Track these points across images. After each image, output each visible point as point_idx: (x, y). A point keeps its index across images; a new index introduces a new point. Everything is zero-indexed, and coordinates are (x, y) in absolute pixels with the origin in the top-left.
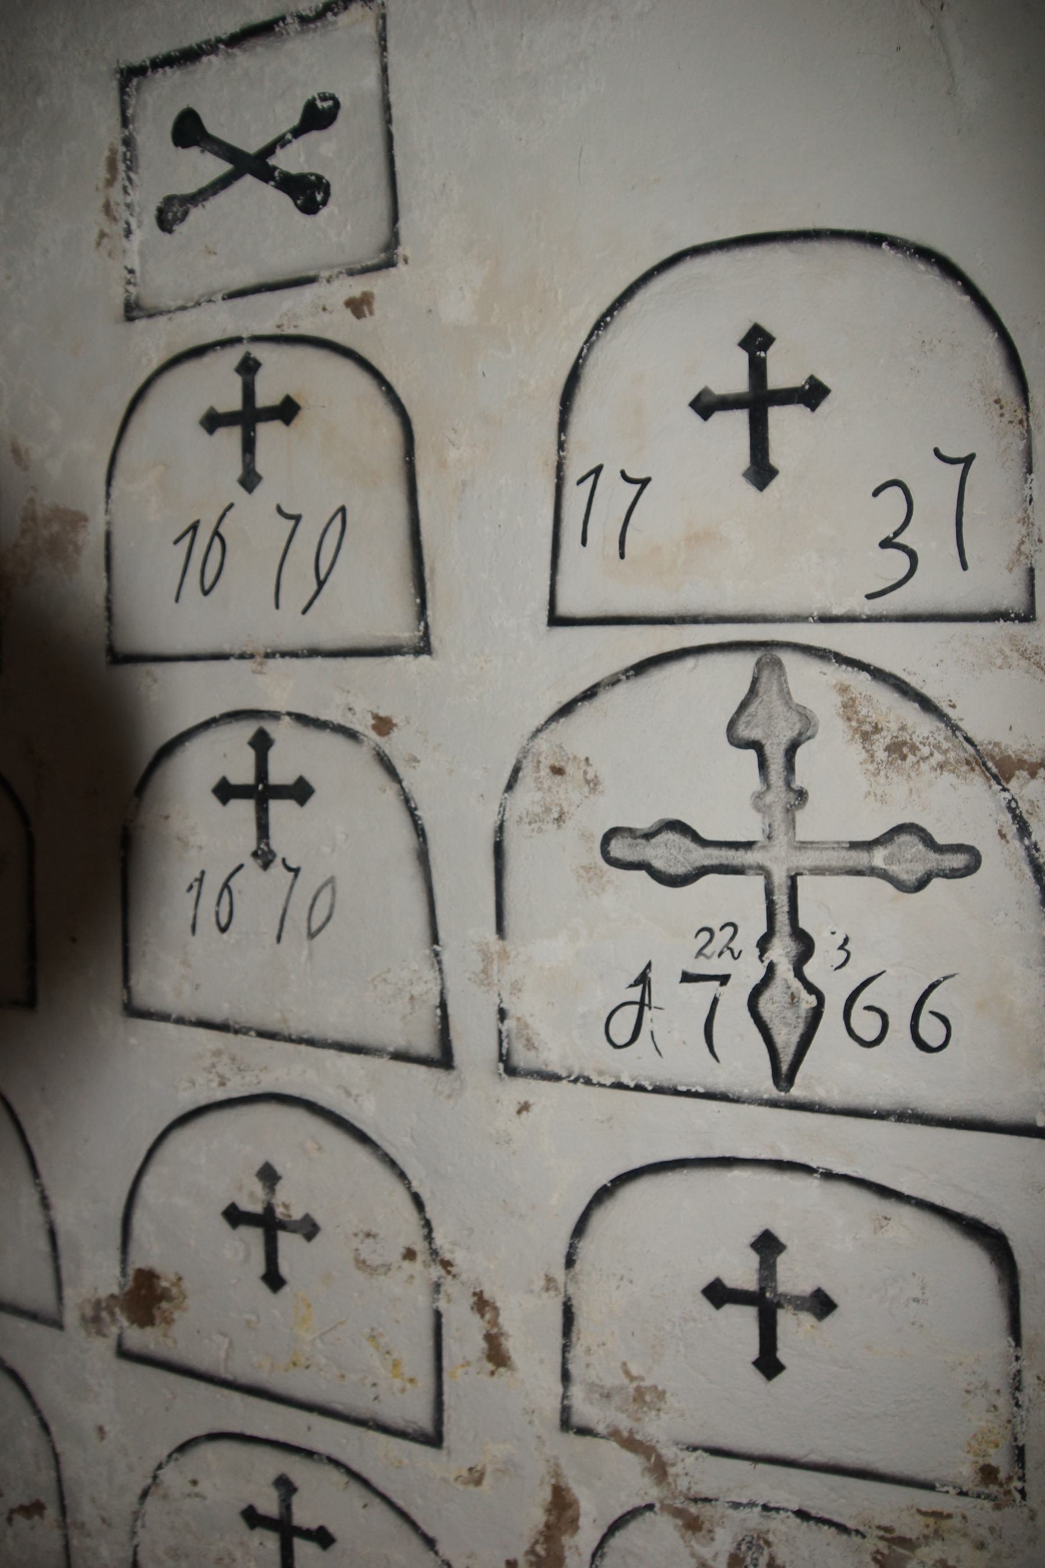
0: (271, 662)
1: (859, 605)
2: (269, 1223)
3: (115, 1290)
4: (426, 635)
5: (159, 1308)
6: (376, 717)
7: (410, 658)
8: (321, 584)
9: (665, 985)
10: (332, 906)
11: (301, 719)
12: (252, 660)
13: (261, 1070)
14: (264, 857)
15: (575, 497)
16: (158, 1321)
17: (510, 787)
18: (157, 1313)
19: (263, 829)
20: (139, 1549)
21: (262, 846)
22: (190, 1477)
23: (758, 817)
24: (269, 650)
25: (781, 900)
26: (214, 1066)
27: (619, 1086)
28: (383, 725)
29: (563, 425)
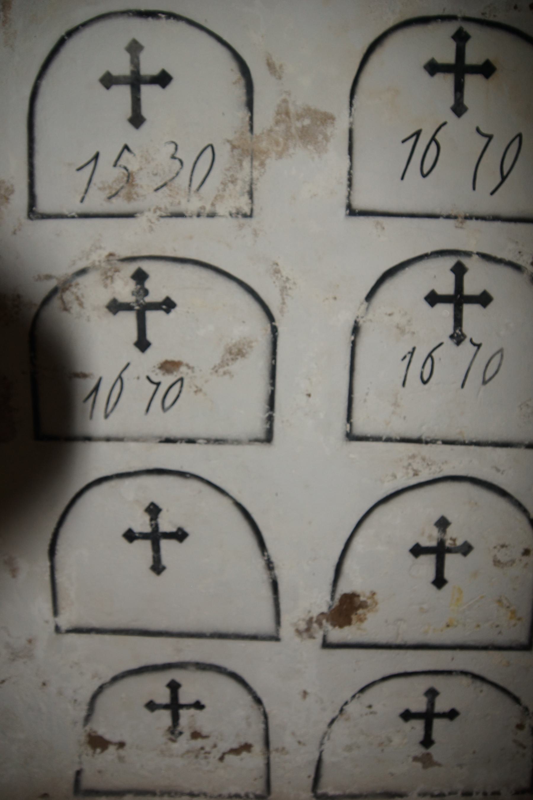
0: (469, 222)
2: (155, 537)
3: (325, 609)
5: (356, 614)
8: (504, 178)
12: (456, 220)
13: (443, 463)
16: (354, 621)
18: (354, 617)
19: (458, 321)
20: (323, 753)
21: (458, 331)
22: (367, 703)
24: (468, 215)
26: (410, 464)
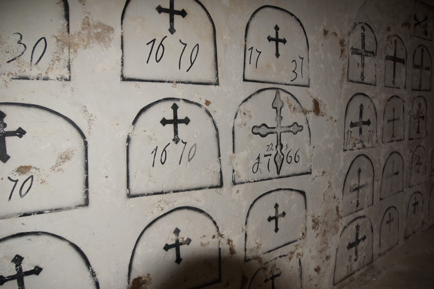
0: (178, 84)
1: (288, 82)
4: (218, 80)
6: (206, 101)
7: (213, 86)
8: (192, 64)
9: (262, 159)
10: (195, 151)
11: (185, 100)
14: (176, 140)
15: (248, 53)
17: (235, 118)
19: (176, 132)
23: (276, 122)
25: (279, 138)
26: (159, 205)
27: (255, 181)
28: (208, 103)
29: (246, 36)
